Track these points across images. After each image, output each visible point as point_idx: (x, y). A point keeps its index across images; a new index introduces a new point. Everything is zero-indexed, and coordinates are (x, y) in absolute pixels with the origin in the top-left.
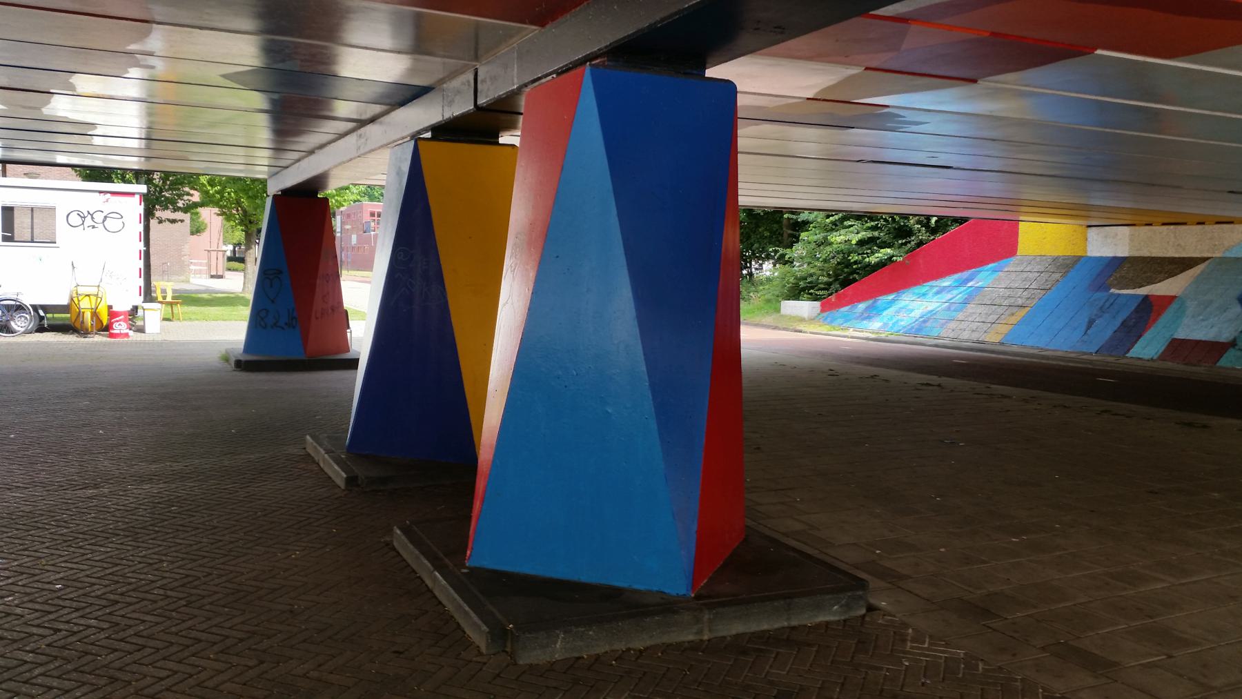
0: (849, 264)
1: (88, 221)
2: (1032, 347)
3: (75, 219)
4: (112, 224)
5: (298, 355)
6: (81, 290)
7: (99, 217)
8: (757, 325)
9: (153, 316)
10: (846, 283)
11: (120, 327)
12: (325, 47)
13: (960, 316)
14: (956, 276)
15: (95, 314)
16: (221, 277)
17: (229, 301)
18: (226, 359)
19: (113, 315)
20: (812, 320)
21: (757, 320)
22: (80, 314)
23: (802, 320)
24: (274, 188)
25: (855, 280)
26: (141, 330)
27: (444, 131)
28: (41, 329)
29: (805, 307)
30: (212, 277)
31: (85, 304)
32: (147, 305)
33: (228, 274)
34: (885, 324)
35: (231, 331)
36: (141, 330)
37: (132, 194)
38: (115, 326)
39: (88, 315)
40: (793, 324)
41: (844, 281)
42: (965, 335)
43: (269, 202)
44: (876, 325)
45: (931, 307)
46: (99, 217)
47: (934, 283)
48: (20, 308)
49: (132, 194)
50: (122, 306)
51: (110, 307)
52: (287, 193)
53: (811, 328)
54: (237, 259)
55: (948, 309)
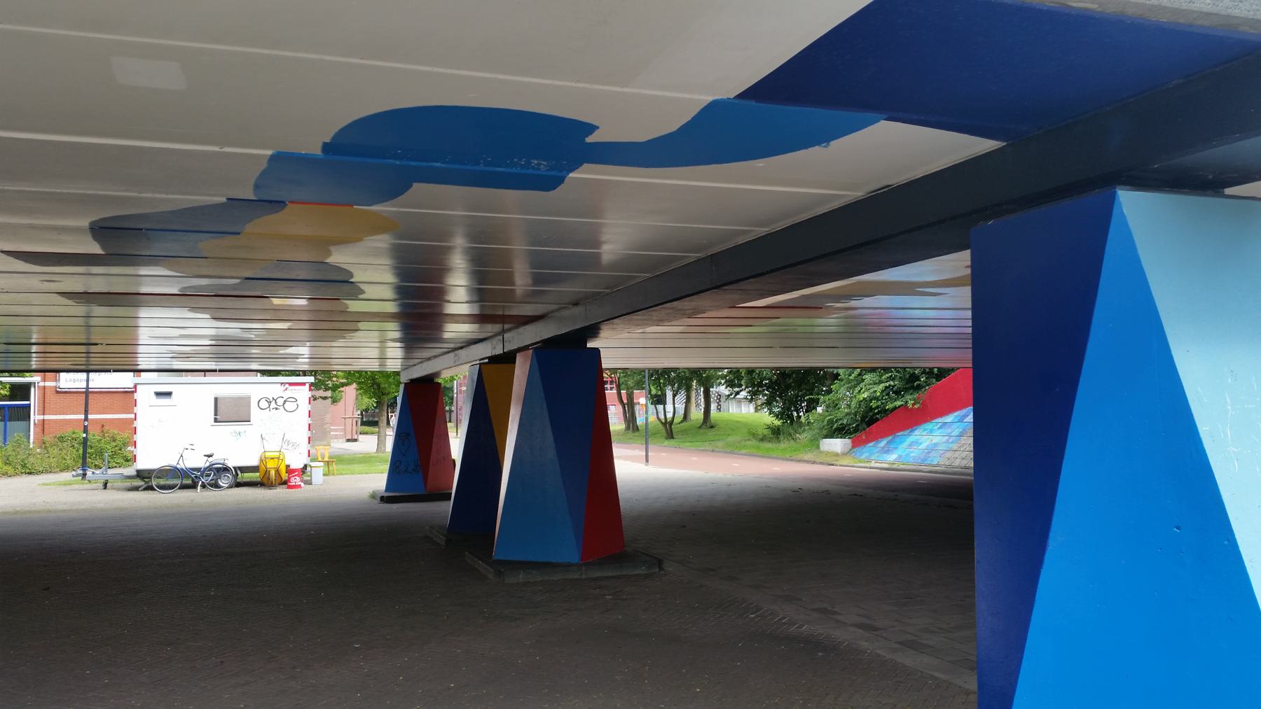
0: (871, 409)
1: (273, 405)
2: (938, 465)
3: (264, 404)
4: (289, 406)
5: (422, 492)
6: (268, 455)
7: (280, 402)
8: (799, 461)
9: (317, 474)
10: (870, 423)
11: (296, 480)
12: (429, 306)
13: (955, 447)
14: (956, 414)
15: (278, 471)
16: (356, 440)
17: (365, 459)
18: (373, 496)
19: (290, 471)
20: (844, 454)
21: (800, 456)
22: (267, 472)
23: (837, 455)
24: (404, 378)
25: (877, 420)
26: (309, 483)
27: (494, 360)
28: (239, 485)
29: (837, 445)
30: (348, 440)
31: (271, 464)
32: (313, 464)
33: (361, 437)
34: (900, 457)
35: (378, 481)
36: (309, 483)
37: (303, 384)
38: (292, 480)
39: (273, 473)
40: (833, 458)
41: (867, 424)
42: (957, 463)
43: (402, 387)
44: (892, 457)
45: (936, 440)
46: (280, 402)
47: (940, 420)
48: (226, 469)
49: (303, 384)
50: (297, 464)
51: (288, 466)
52: (413, 381)
53: (845, 461)
54: (369, 421)
55: (947, 442)
